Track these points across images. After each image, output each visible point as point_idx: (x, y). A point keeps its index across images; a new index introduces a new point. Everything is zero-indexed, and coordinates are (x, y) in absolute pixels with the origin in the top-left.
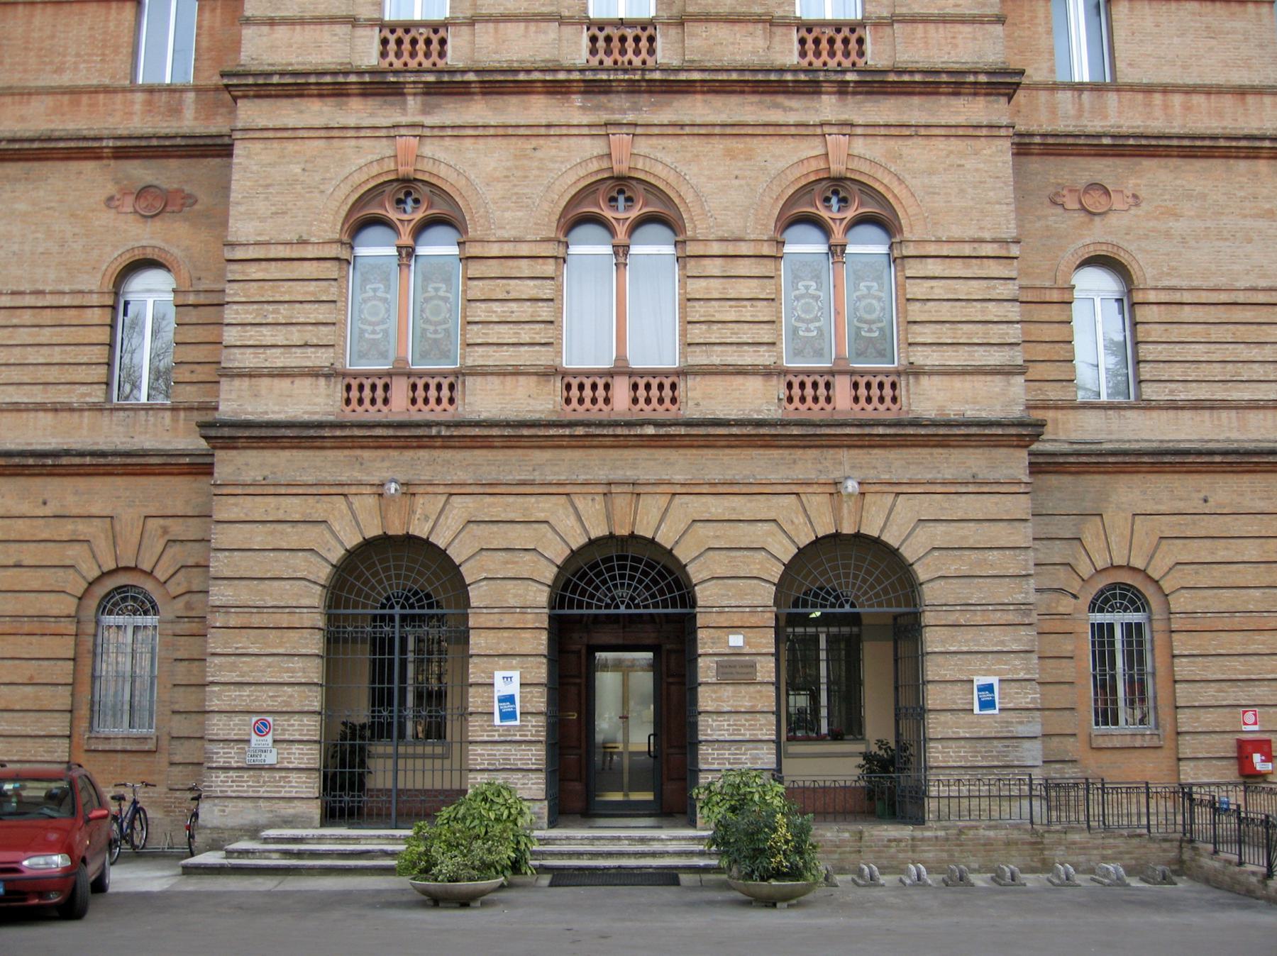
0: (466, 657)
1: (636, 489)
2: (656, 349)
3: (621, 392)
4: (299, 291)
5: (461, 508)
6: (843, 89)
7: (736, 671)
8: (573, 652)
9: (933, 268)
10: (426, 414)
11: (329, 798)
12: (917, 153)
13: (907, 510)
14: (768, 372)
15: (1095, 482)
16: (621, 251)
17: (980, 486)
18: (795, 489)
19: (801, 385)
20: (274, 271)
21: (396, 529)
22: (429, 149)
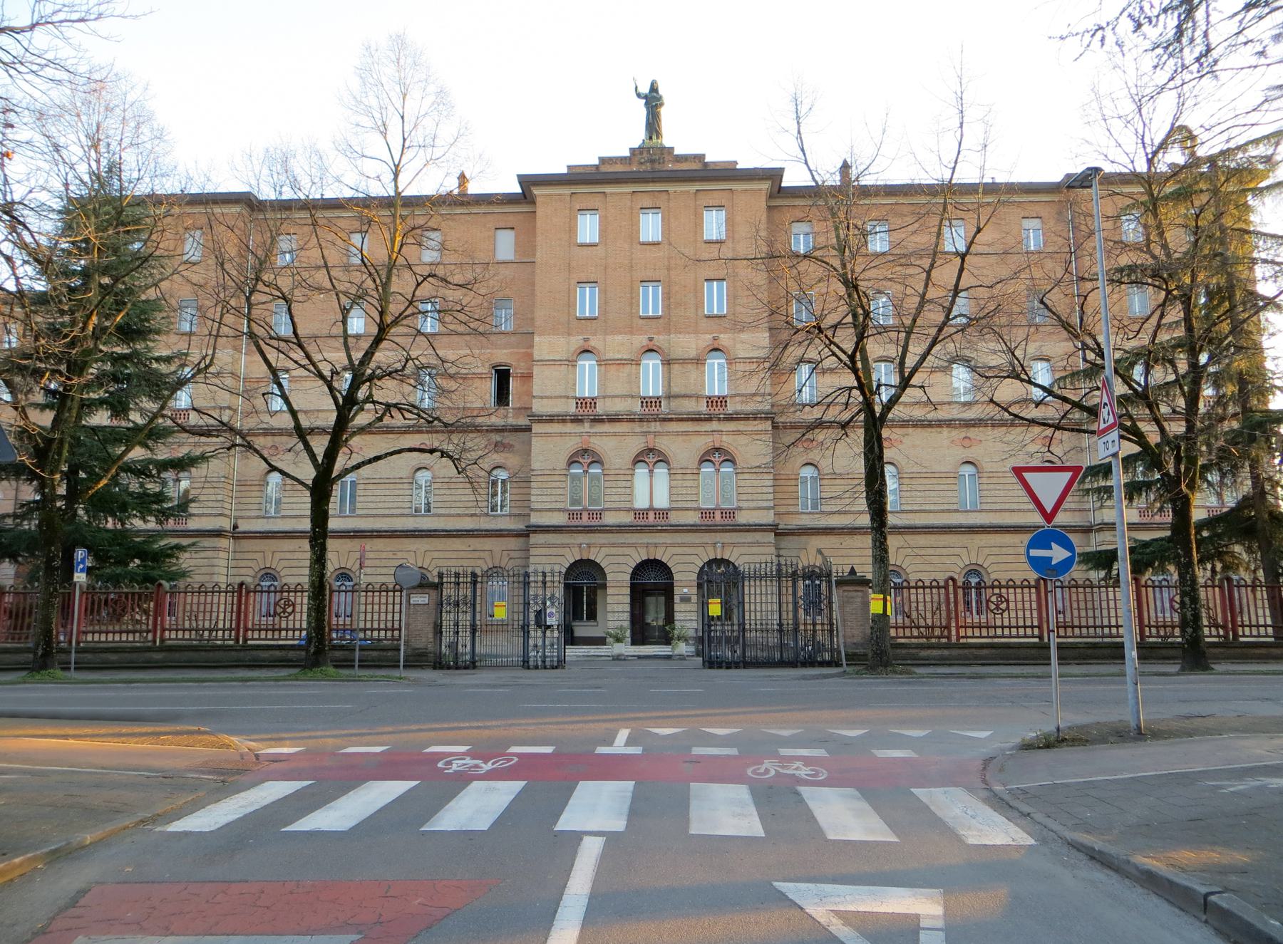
0: (606, 595)
1: (656, 546)
2: (662, 501)
3: (651, 515)
4: (554, 485)
5: (604, 551)
6: (719, 419)
7: (686, 600)
8: (240, 612)
9: (747, 476)
10: (593, 523)
11: (1241, 364)
12: (742, 440)
13: (737, 551)
14: (695, 509)
15: (804, 538)
16: (651, 471)
17: (759, 544)
18: (703, 545)
19: (706, 513)
20: (546, 478)
21: (585, 558)
22: (593, 440)
